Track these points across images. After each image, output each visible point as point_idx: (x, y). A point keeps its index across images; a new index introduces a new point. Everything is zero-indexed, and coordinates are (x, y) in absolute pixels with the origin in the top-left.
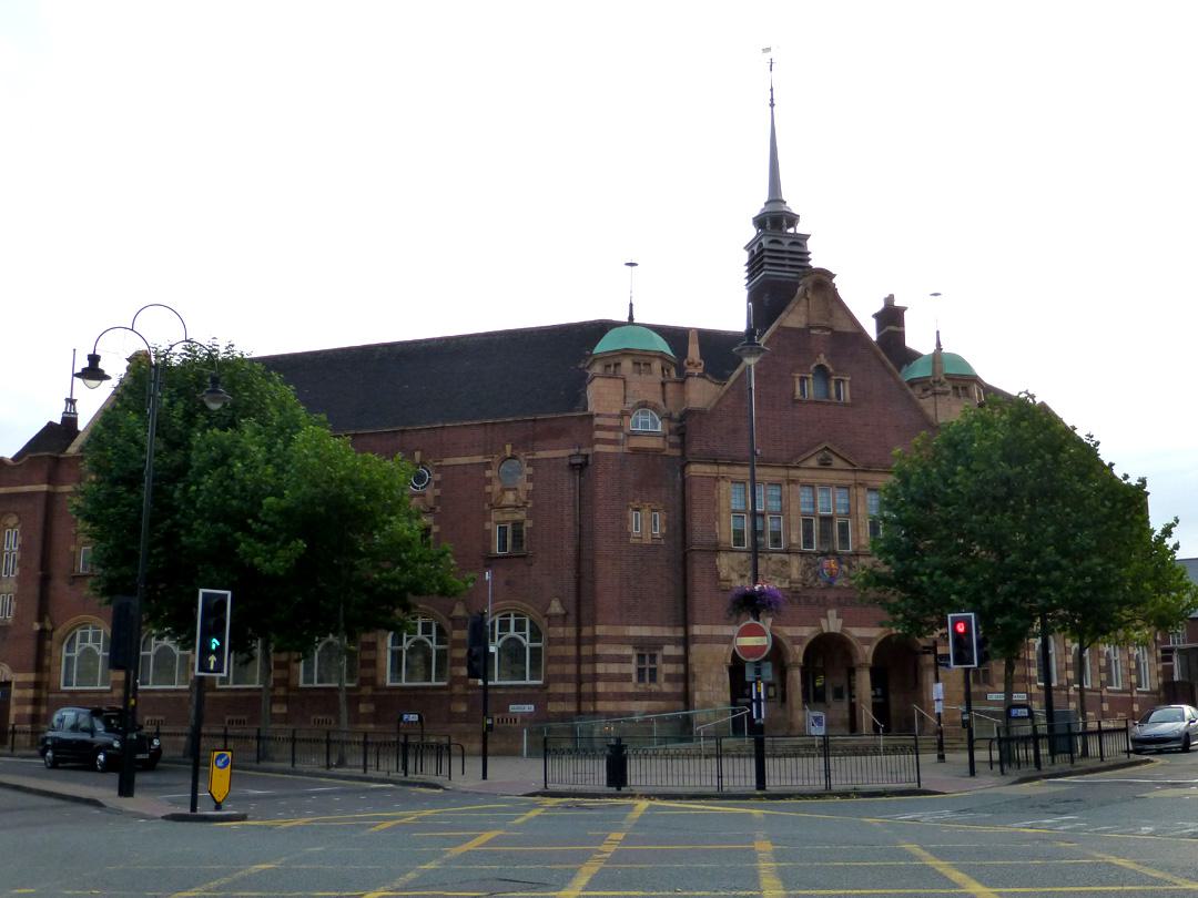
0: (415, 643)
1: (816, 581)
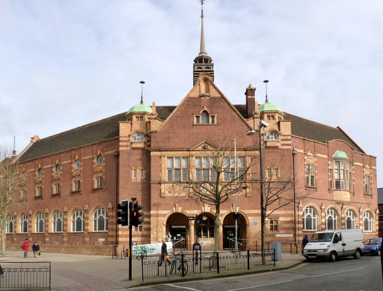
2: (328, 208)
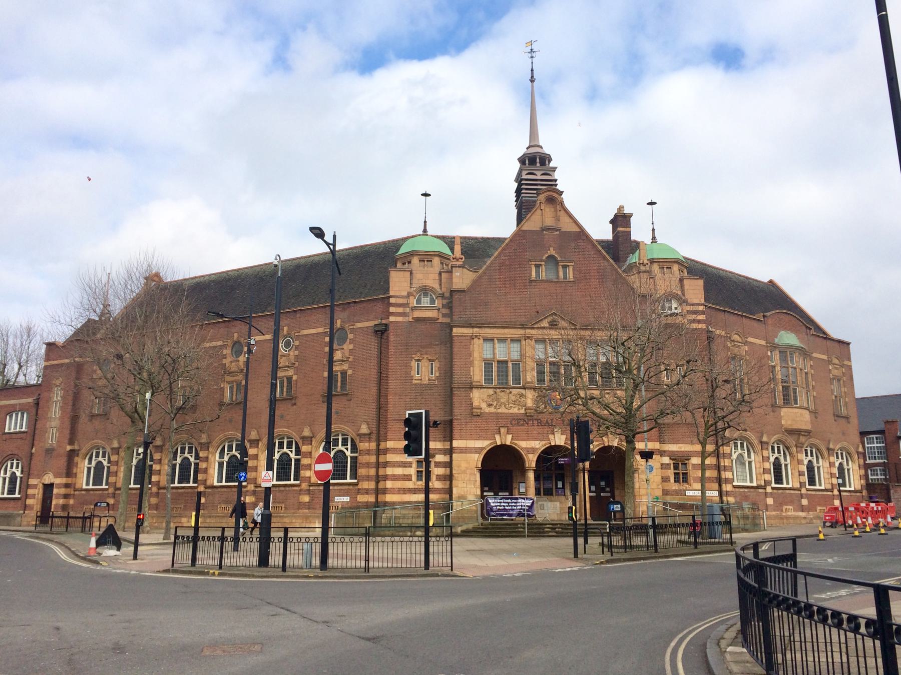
0: (283, 454)
1: (545, 407)
2: (773, 440)
